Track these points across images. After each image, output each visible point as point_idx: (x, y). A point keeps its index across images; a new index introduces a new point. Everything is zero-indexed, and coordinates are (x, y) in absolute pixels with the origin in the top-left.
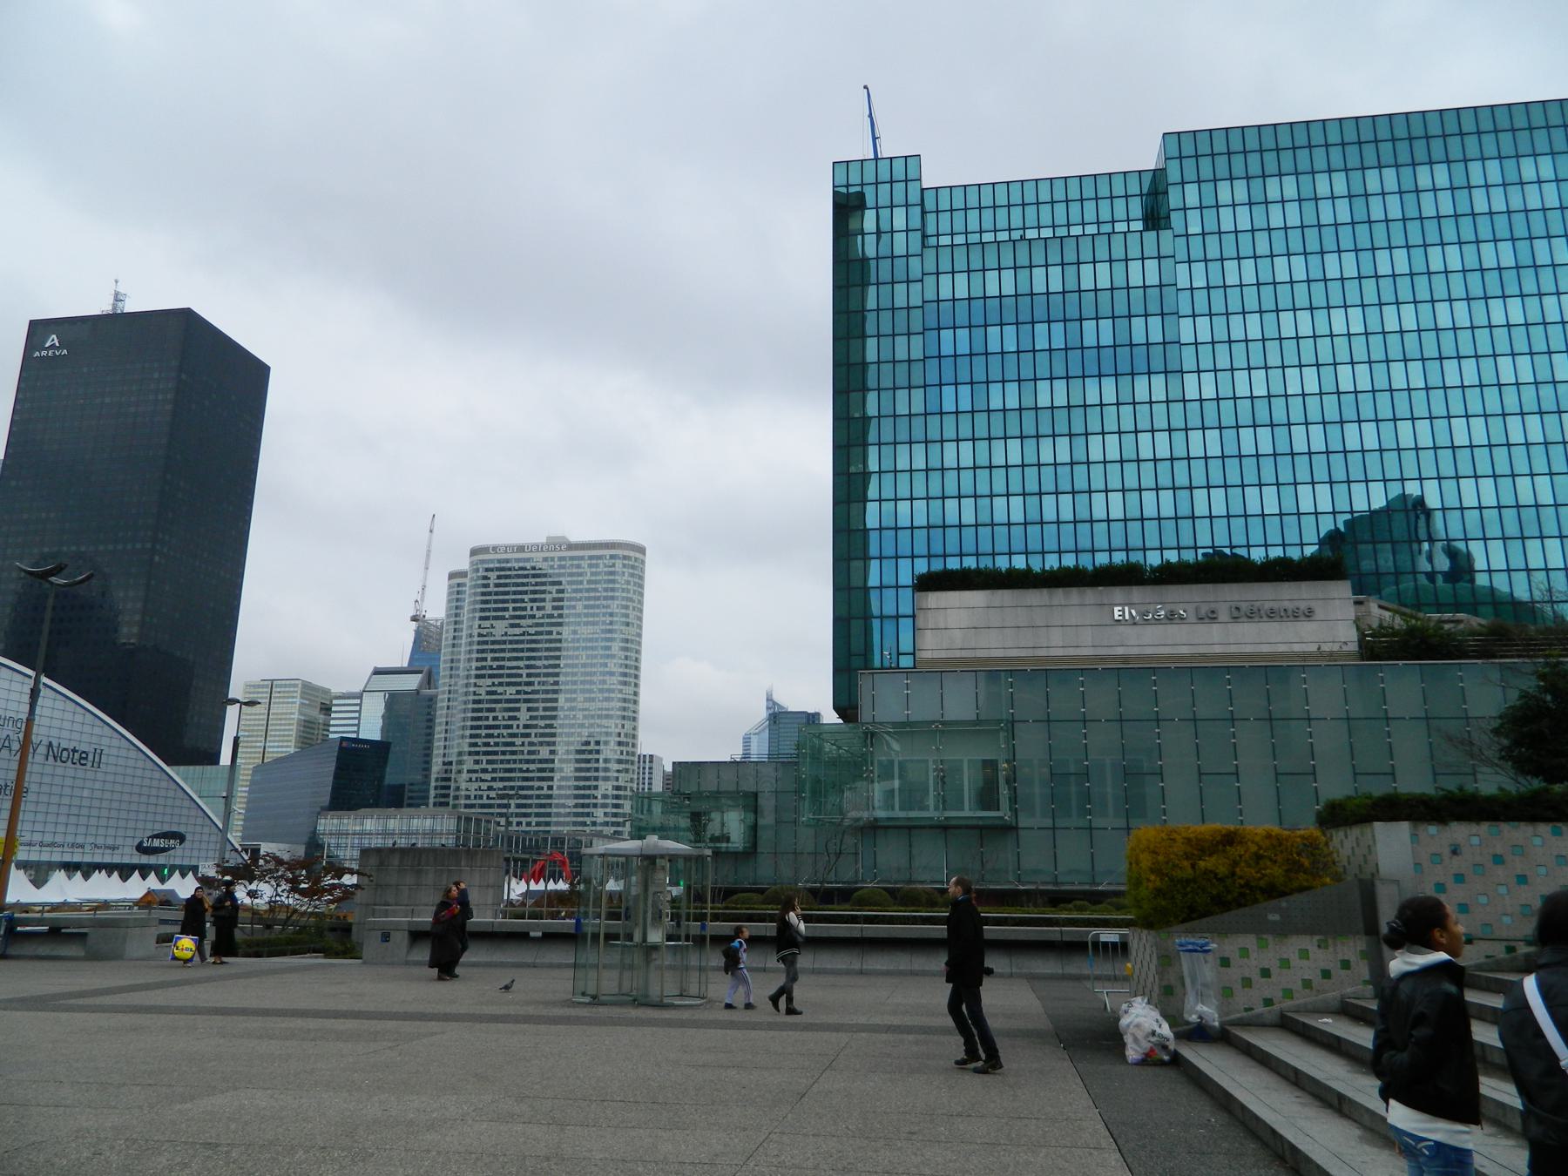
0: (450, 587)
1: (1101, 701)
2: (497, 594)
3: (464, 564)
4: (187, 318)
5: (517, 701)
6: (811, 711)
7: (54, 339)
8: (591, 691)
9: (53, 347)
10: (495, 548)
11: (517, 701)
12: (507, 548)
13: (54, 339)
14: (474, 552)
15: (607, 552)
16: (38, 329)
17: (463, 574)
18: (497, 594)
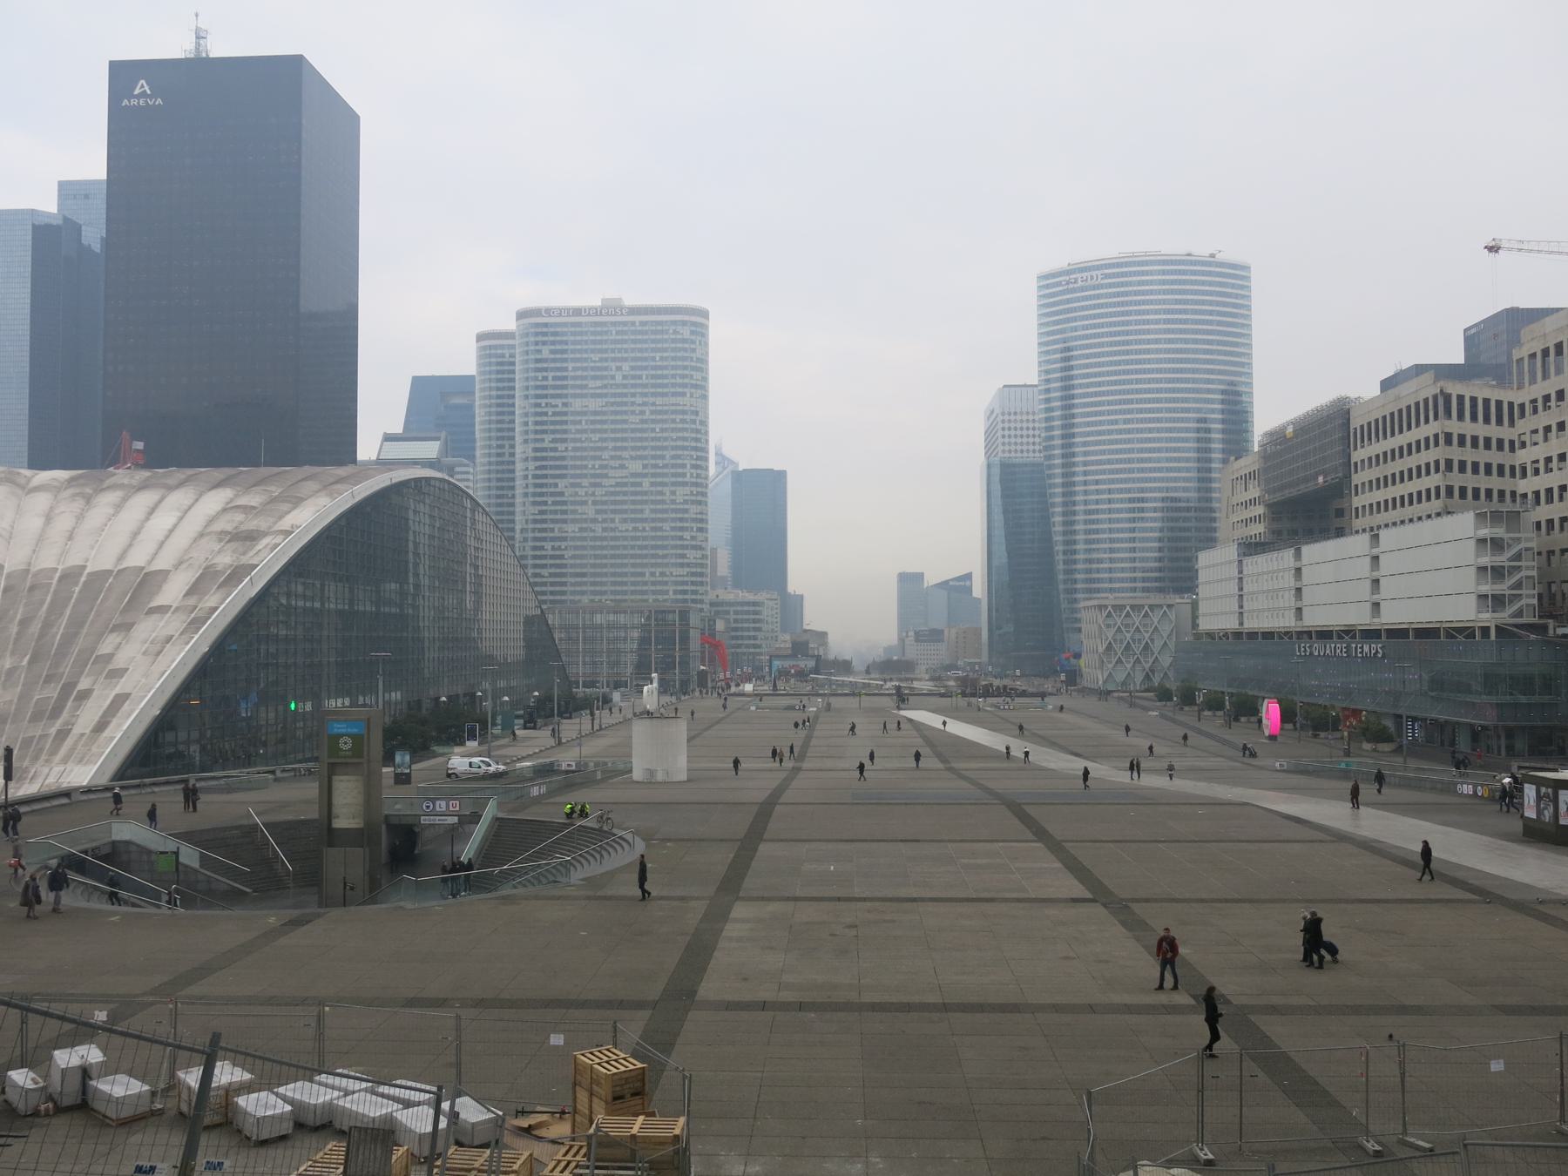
7: (142, 86)
13: (142, 86)
14: (522, 315)
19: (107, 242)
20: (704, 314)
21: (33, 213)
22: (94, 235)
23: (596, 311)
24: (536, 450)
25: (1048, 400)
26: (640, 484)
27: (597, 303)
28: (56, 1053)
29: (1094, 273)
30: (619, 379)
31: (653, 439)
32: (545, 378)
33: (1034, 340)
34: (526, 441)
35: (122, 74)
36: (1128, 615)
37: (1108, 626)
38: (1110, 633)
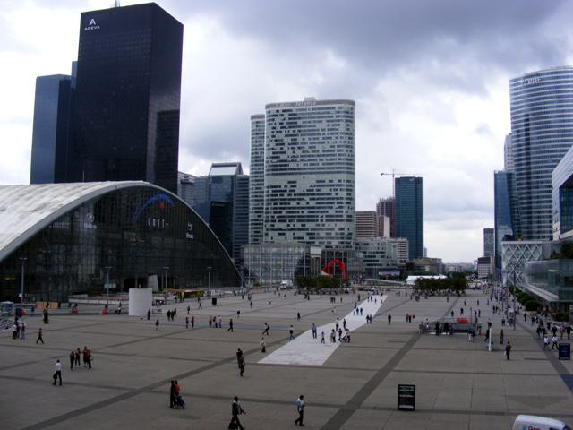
0: (252, 123)
1: (342, 128)
2: (308, 216)
3: (264, 112)
4: (153, 6)
5: (281, 208)
6: (417, 176)
7: (93, 21)
8: (341, 203)
9: (93, 25)
10: (279, 104)
11: (281, 208)
12: (285, 104)
13: (93, 21)
14: (268, 107)
15: (336, 106)
16: (85, 17)
17: (262, 116)
18: (308, 216)
19: (77, 85)
20: (353, 103)
21: (60, 75)
22: (73, 85)
23: (302, 104)
24: (274, 153)
25: (518, 141)
26: (330, 234)
27: (302, 100)
28: (192, 165)
29: (535, 78)
30: (321, 165)
31: (314, 118)
32: (276, 204)
33: (509, 117)
34: (269, 124)
35: (85, 17)
36: (527, 249)
37: (509, 255)
38: (509, 258)
